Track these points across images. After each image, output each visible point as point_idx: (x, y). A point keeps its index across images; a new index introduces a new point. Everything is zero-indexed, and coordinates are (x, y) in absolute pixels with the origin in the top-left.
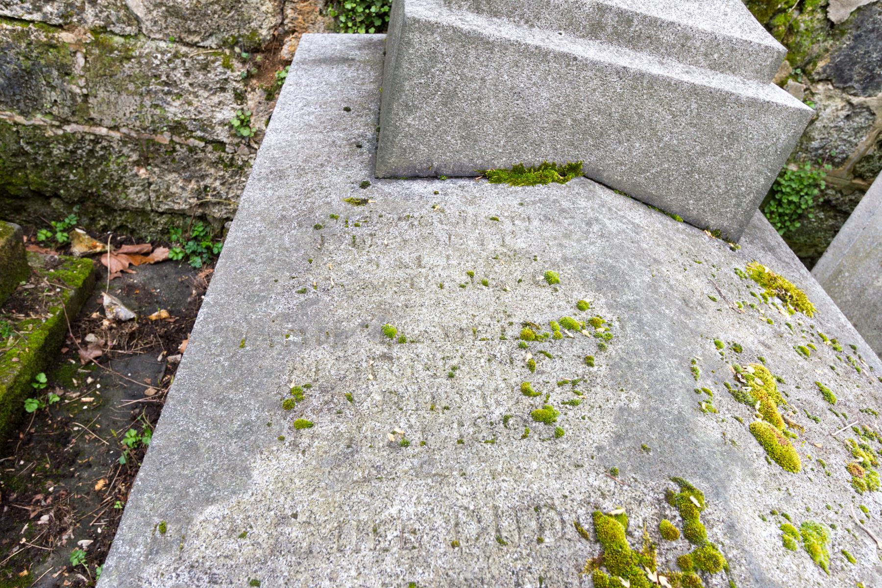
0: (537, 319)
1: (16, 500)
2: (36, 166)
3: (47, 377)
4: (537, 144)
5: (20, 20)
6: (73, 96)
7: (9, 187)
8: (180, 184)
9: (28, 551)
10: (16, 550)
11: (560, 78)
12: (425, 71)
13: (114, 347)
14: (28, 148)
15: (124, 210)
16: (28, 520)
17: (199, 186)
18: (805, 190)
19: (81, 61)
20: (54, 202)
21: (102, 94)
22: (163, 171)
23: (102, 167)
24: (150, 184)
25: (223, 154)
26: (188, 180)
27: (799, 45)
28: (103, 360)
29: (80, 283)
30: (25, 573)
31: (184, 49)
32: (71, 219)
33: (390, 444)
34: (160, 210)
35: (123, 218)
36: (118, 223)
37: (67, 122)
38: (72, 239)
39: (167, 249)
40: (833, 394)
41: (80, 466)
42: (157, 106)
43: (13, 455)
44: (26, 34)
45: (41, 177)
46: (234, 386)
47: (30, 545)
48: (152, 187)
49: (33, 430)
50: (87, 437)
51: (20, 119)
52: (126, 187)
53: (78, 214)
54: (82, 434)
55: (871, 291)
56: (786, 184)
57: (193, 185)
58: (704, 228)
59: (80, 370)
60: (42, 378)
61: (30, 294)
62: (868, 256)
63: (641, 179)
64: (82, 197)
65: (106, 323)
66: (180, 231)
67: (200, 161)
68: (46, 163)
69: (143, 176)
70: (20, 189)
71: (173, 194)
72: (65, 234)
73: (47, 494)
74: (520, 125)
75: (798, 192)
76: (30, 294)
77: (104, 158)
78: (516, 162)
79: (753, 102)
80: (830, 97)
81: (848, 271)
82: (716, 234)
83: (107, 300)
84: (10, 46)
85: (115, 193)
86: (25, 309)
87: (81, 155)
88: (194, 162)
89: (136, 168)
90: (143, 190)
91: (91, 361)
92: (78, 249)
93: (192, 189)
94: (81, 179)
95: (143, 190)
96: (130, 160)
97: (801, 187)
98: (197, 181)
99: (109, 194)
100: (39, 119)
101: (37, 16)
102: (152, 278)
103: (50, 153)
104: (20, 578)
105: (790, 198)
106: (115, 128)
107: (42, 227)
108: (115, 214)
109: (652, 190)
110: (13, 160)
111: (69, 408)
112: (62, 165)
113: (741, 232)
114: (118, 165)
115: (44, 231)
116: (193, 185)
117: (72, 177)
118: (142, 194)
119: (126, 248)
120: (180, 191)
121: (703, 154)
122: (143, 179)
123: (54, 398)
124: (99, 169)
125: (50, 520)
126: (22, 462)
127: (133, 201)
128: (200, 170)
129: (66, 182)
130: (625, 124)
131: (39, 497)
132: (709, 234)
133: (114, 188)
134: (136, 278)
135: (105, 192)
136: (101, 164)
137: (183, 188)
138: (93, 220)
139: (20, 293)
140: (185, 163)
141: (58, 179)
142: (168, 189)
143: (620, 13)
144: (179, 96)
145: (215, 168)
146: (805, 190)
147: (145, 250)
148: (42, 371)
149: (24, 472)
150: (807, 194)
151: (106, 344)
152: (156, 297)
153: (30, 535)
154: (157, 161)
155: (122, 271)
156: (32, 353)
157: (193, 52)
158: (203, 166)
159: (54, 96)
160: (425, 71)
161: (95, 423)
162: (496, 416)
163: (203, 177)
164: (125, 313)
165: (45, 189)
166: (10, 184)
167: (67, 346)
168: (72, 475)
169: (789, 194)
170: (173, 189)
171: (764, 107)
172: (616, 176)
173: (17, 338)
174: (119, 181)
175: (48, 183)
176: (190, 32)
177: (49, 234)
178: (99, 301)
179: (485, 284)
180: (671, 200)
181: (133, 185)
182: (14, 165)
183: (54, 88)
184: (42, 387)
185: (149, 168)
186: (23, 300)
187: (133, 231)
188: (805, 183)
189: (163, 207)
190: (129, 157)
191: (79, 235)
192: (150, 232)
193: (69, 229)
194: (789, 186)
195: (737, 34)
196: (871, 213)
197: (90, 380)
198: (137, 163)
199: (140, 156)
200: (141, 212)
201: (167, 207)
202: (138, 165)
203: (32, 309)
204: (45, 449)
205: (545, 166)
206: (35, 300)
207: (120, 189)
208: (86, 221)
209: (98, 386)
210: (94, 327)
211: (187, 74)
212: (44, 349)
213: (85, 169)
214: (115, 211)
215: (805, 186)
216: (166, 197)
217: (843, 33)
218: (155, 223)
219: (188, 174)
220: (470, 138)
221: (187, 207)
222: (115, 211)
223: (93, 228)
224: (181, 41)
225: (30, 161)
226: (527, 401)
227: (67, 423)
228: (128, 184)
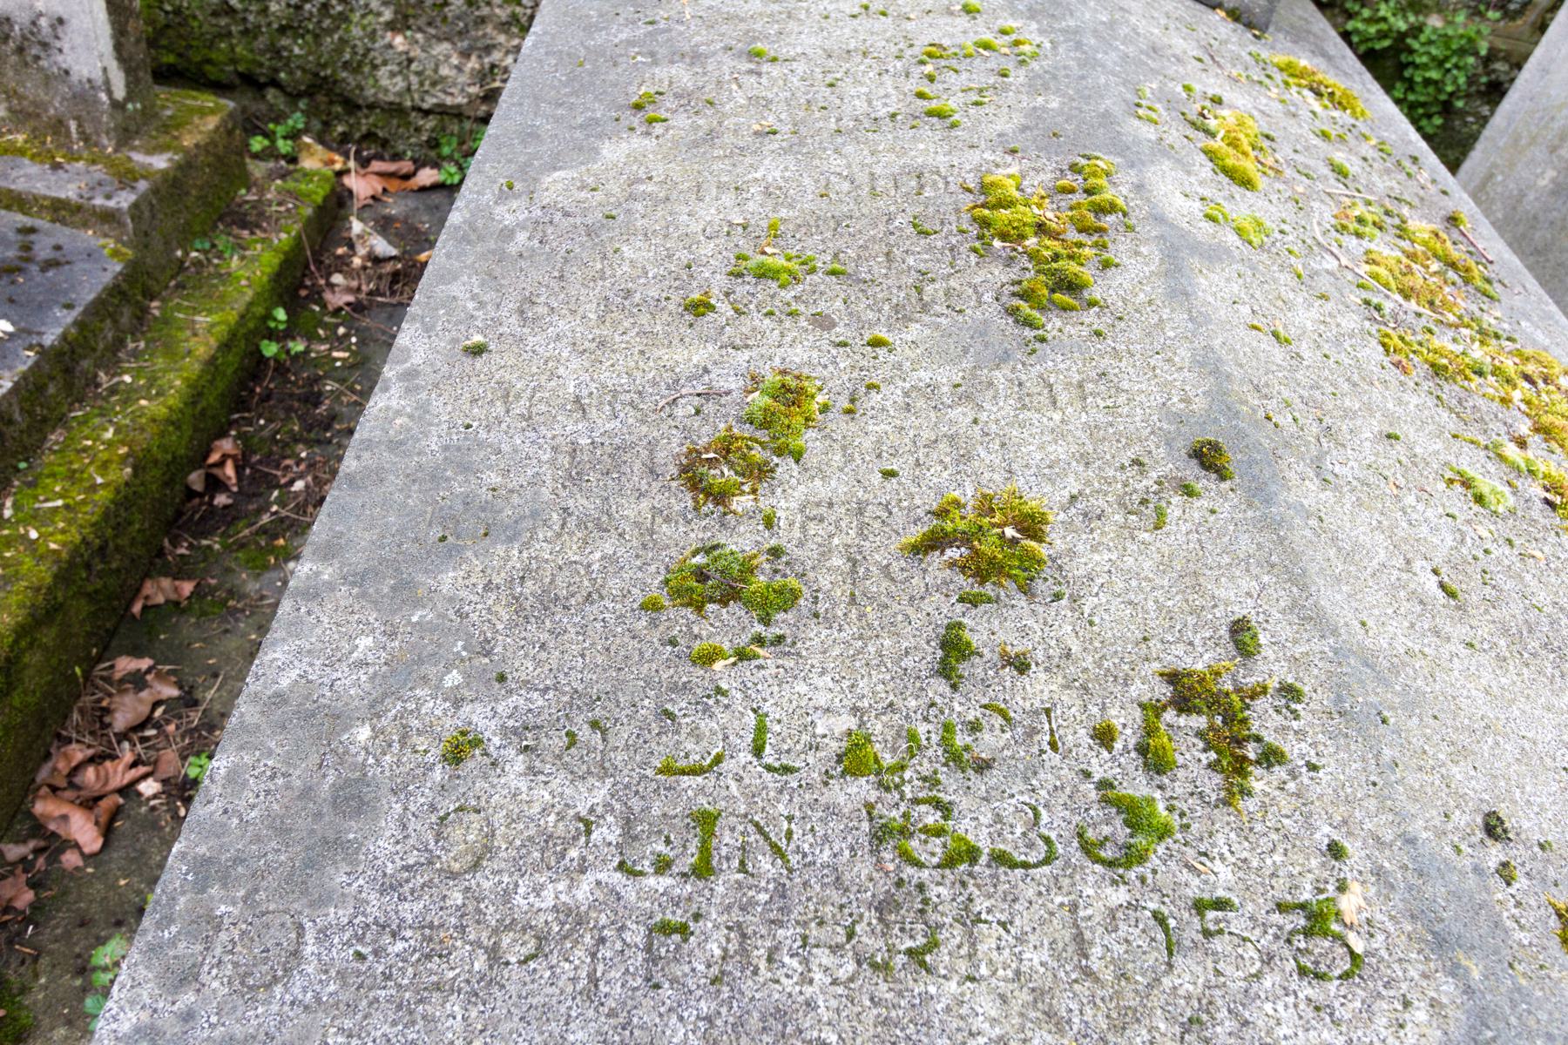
0: (946, 42)
1: (260, 462)
2: (246, 32)
3: (287, 313)
7: (208, 68)
8: (455, 60)
9: (282, 520)
10: (266, 518)
13: (370, 293)
15: (372, 107)
16: (278, 486)
17: (482, 65)
18: (1454, 60)
20: (271, 94)
22: (429, 38)
23: (341, 32)
24: (410, 61)
25: (518, 10)
26: (466, 55)
28: (357, 307)
29: (319, 200)
30: (281, 542)
32: (297, 120)
33: (756, 133)
34: (425, 106)
35: (371, 120)
36: (364, 129)
38: (300, 151)
39: (435, 171)
40: (1347, 165)
41: (339, 431)
43: (249, 411)
45: (252, 51)
46: (575, 93)
47: (284, 513)
48: (414, 66)
49: (272, 386)
50: (344, 399)
52: (375, 67)
53: (307, 114)
54: (336, 395)
55: (1531, 197)
56: (1422, 50)
57: (473, 64)
59: (327, 319)
60: (281, 314)
61: (253, 207)
62: (1533, 141)
64: (313, 86)
65: (357, 262)
66: (455, 141)
67: (482, 20)
68: (259, 27)
69: (401, 48)
70: (222, 71)
71: (443, 79)
72: (289, 142)
73: (299, 461)
75: (1440, 63)
76: (253, 207)
77: (344, 18)
81: (1502, 173)
83: (357, 227)
85: (359, 77)
86: (252, 226)
87: (311, 13)
88: (476, 23)
89: (389, 34)
90: (400, 72)
91: (341, 309)
92: (308, 163)
93: (473, 69)
94: (310, 53)
95: (400, 72)
96: (382, 19)
97: (1448, 53)
98: (480, 57)
99: (351, 80)
102: (417, 209)
104: (275, 547)
105: (1428, 75)
107: (255, 134)
108: (360, 114)
110: (214, 21)
111: (316, 363)
112: (283, 30)
114: (364, 28)
115: (259, 138)
116: (473, 64)
117: (297, 50)
118: (399, 79)
119: (377, 166)
120: (453, 73)
122: (400, 54)
123: (298, 346)
124: (336, 37)
125: (307, 487)
126: (262, 422)
127: (386, 91)
128: (485, 35)
129: (289, 58)
131: (288, 462)
132: (1223, 14)
133: (356, 69)
134: (394, 208)
135: (344, 74)
136: (338, 28)
137: (459, 69)
138: (326, 124)
139: (240, 206)
140: (461, 24)
141: (277, 53)
142: (436, 71)
145: (506, 32)
146: (1454, 60)
147: (404, 171)
148: (277, 305)
149: (266, 433)
150: (1456, 66)
151: (359, 289)
152: (425, 233)
153: (281, 502)
154: (422, 22)
155: (373, 197)
156: (265, 279)
158: (489, 29)
161: (356, 382)
162: (883, 112)
163: (488, 49)
164: (382, 247)
165: (258, 71)
166: (209, 61)
167: (306, 287)
168: (329, 442)
169: (1425, 67)
170: (445, 71)
173: (242, 258)
174: (364, 55)
175: (262, 59)
177: (266, 143)
178: (345, 235)
179: (884, 14)
181: (385, 63)
182: (215, 29)
184: (282, 327)
185: (409, 33)
186: (245, 215)
187: (385, 143)
188: (1454, 46)
189: (429, 102)
190: (379, 14)
191: (308, 146)
192: (410, 145)
193: (294, 136)
194: (1428, 53)
196: (1545, 71)
197: (341, 331)
198: (391, 26)
199: (396, 12)
200: (396, 110)
201: (435, 101)
202: (393, 30)
203: (259, 226)
204: (289, 410)
206: (261, 214)
207: (366, 69)
208: (316, 125)
209: (354, 340)
210: (342, 265)
212: (277, 277)
213: (317, 37)
214: (359, 107)
215: (1455, 52)
216: (434, 84)
218: (418, 130)
219: (465, 44)
221: (465, 101)
222: (359, 107)
223: (327, 138)
225: (236, 23)
226: (920, 102)
227: (317, 380)
228: (378, 61)
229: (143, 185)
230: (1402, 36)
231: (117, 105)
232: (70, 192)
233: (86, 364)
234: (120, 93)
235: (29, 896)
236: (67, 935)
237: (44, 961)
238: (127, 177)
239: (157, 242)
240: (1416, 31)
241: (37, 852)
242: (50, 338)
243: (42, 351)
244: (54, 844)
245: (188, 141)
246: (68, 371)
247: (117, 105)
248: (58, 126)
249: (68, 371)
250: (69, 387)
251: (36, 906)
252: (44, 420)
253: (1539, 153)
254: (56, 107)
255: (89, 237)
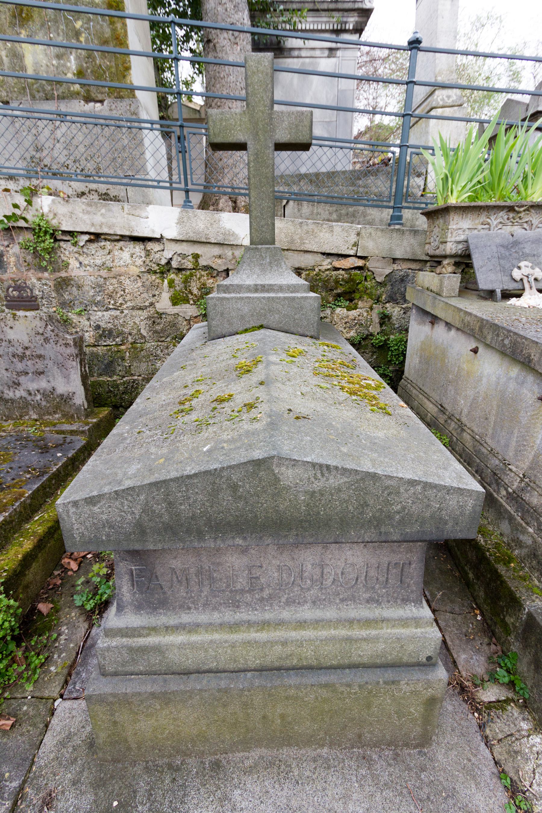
4: (249, 322)
5: (109, 345)
6: (126, 366)
11: (249, 303)
12: (214, 309)
14: (112, 389)
19: (128, 354)
20: (120, 409)
21: (135, 364)
27: (371, 292)
31: (160, 343)
37: (124, 377)
42: (153, 365)
44: (110, 349)
51: (109, 379)
58: (307, 336)
63: (281, 325)
74: (242, 317)
77: (137, 388)
78: (245, 328)
79: (302, 297)
80: (393, 308)
82: (311, 337)
84: (106, 354)
100: (115, 378)
101: (114, 343)
103: (119, 390)
106: (140, 376)
109: (286, 328)
112: (123, 393)
113: (319, 335)
121: (295, 314)
130: (270, 311)
143: (261, 285)
144: (160, 359)
157: (163, 343)
159: (120, 368)
160: (214, 309)
171: (306, 298)
172: (274, 326)
176: (161, 337)
180: (292, 329)
183: (119, 365)
195: (295, 283)
205: (253, 327)
211: (162, 351)
217: (386, 285)
220: (231, 324)
224: (159, 341)
229: (91, 425)
230: (385, 340)
231: (85, 409)
232: (74, 428)
233: (77, 463)
234: (86, 407)
235: (60, 581)
236: (69, 589)
237: (63, 595)
238: (87, 424)
239: (93, 438)
240: (389, 339)
241: (62, 572)
242: (70, 455)
243: (68, 458)
244: (66, 570)
245: (101, 416)
246: (73, 463)
247: (85, 409)
248: (72, 417)
249: (73, 463)
250: (73, 467)
251: (61, 584)
252: (68, 474)
253: (415, 356)
254: (72, 411)
255: (78, 437)
